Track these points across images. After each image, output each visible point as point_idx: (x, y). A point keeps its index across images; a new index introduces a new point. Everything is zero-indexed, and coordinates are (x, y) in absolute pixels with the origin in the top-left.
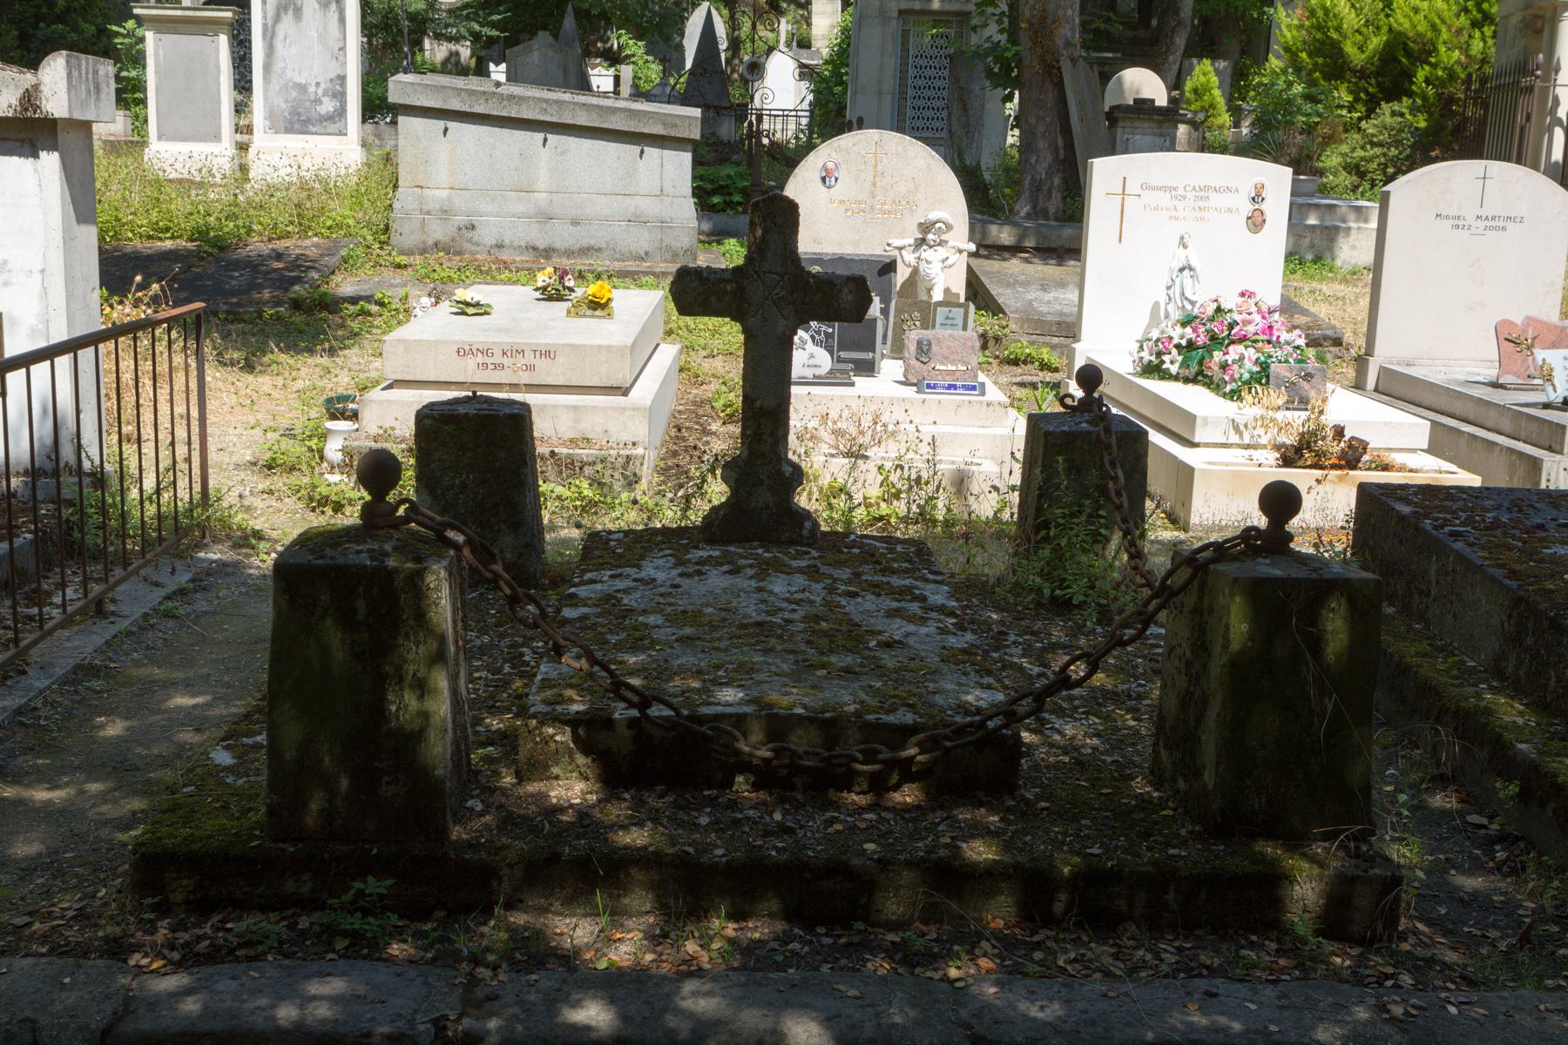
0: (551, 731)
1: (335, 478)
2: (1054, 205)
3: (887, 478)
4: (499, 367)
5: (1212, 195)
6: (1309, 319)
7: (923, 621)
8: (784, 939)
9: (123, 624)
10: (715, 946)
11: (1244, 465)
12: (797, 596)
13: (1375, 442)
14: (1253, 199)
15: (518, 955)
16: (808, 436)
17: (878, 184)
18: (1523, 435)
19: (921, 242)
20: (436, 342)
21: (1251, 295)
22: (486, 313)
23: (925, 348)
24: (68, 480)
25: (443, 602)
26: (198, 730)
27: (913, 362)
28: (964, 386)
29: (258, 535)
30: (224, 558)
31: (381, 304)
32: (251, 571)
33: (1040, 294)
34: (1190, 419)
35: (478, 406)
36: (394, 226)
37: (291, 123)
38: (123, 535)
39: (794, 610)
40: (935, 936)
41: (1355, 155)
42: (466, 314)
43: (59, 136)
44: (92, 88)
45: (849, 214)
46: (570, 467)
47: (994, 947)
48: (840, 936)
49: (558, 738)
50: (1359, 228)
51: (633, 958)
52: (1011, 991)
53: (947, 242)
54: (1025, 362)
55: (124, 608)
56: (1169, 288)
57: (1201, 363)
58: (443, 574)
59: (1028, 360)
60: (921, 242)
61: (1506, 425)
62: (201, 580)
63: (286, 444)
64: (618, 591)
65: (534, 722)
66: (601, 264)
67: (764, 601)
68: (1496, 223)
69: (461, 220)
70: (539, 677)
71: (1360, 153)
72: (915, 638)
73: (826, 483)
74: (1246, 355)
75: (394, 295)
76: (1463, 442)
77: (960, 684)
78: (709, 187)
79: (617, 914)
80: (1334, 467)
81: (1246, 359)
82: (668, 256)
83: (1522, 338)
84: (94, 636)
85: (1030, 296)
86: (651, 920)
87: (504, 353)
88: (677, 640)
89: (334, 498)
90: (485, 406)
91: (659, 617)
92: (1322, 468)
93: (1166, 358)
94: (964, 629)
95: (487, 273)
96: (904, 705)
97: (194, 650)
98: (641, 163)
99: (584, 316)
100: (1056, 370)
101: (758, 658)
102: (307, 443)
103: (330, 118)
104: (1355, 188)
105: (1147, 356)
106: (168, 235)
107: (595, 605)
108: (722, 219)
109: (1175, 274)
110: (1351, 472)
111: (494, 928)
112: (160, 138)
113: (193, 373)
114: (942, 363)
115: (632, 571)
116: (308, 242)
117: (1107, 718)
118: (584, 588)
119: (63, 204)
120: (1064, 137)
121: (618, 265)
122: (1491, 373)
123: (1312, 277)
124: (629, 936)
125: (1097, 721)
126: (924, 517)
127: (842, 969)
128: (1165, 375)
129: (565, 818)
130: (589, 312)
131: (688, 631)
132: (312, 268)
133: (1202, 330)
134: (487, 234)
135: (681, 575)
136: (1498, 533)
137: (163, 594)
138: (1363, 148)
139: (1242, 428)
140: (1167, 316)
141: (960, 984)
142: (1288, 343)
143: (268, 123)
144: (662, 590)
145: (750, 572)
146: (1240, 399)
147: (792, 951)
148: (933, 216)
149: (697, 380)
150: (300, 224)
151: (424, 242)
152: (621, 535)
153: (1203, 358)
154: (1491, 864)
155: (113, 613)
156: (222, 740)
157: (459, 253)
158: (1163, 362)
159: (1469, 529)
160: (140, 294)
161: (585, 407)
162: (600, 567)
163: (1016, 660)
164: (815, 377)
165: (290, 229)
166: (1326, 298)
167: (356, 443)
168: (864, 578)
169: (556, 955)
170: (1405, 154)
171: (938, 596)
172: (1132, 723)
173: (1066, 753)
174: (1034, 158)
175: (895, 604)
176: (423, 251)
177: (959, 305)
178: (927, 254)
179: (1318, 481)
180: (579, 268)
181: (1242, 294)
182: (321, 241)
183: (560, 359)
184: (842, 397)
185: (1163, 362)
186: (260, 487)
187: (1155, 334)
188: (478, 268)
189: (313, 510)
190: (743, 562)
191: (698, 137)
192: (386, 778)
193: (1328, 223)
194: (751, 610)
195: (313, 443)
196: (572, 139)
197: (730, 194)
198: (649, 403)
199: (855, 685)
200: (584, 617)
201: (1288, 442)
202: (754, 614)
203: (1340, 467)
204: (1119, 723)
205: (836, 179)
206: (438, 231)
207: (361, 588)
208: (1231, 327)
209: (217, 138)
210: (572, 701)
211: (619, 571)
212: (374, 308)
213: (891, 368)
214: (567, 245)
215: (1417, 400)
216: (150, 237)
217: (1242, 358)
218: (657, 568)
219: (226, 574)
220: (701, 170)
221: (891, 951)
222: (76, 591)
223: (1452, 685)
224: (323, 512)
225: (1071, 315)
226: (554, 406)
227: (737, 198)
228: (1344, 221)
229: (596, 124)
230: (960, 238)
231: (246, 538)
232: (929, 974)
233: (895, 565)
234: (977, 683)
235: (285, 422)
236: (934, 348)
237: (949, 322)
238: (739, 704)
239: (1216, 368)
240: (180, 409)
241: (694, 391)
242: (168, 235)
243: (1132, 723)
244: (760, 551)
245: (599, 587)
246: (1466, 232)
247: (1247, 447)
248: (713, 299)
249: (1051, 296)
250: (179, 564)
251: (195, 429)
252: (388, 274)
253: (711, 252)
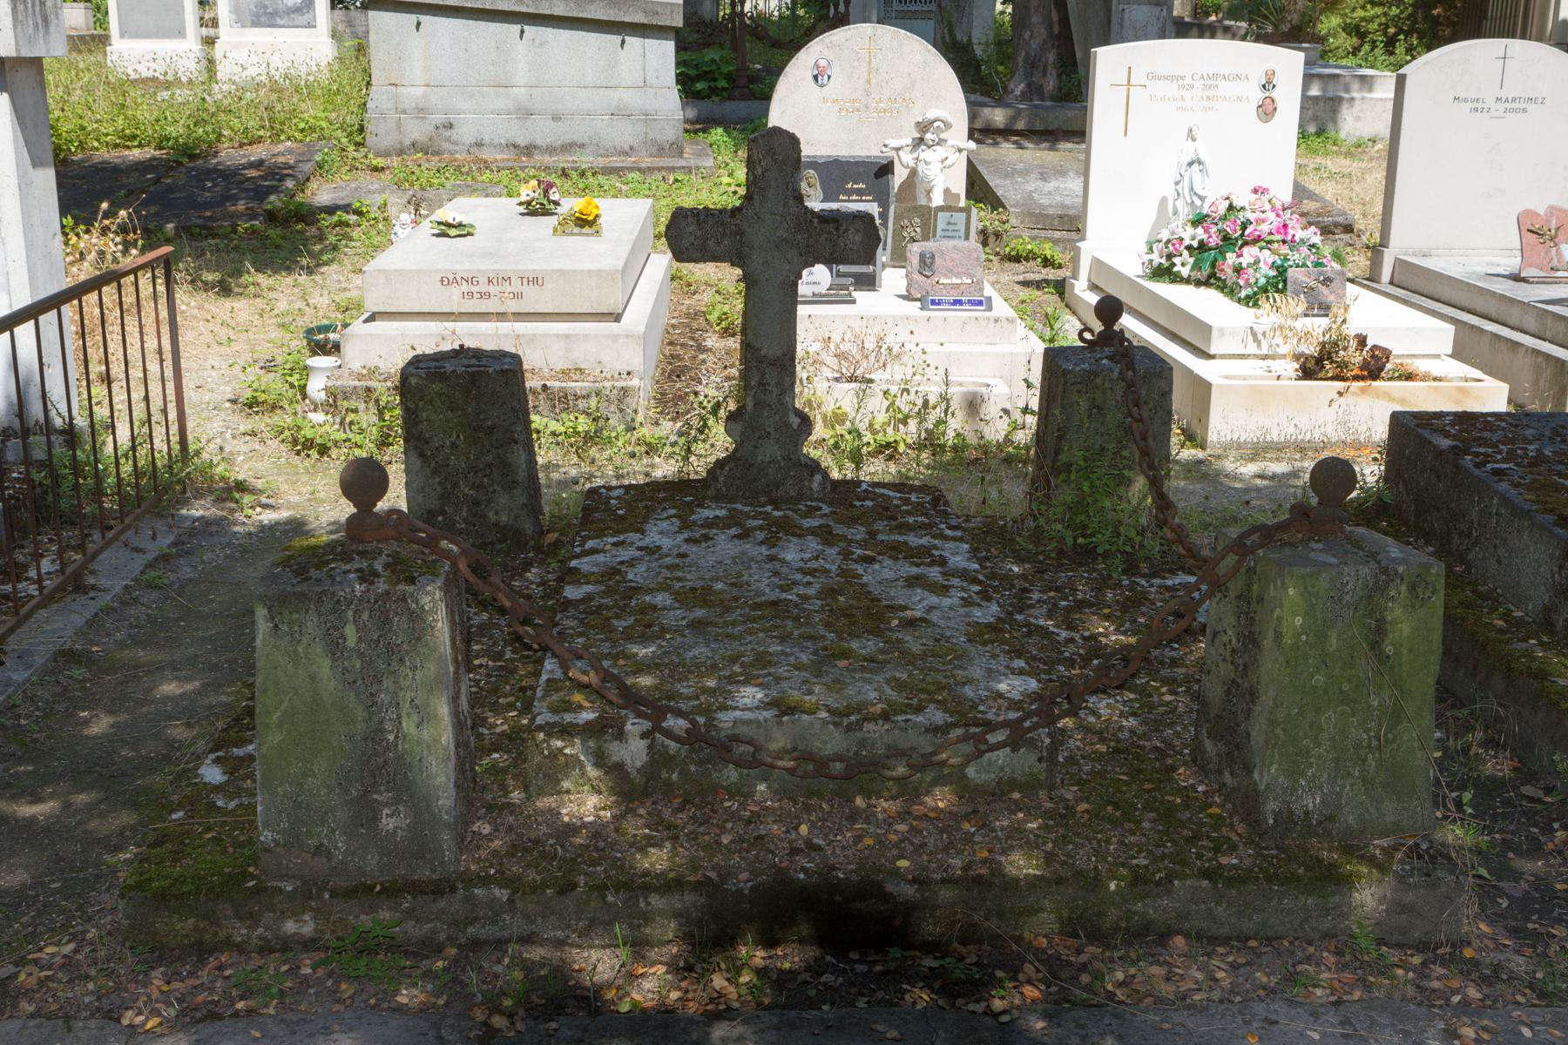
0: (559, 744)
1: (319, 417)
2: (1050, 84)
3: (893, 403)
5: (1221, 83)
6: (1318, 205)
7: (944, 590)
8: (816, 968)
9: (104, 600)
10: (745, 979)
11: (1263, 378)
12: (814, 564)
13: (1398, 347)
14: (1264, 86)
15: (535, 998)
16: (810, 361)
17: (874, 81)
18: (1548, 335)
19: (920, 141)
20: (419, 271)
21: (1264, 191)
22: (469, 234)
23: (928, 261)
24: (37, 440)
25: (440, 624)
26: (188, 725)
27: (916, 276)
28: (970, 302)
29: (241, 487)
30: (207, 514)
31: (359, 213)
32: (237, 529)
33: (1040, 183)
34: (1206, 329)
35: (466, 362)
36: (369, 127)
37: (258, 16)
38: (98, 492)
39: (809, 584)
40: (975, 959)
41: (1355, 15)
42: (448, 236)
43: (8, 76)
44: (40, 21)
45: (843, 113)
46: (562, 401)
47: (1038, 971)
48: (874, 963)
49: (567, 751)
50: (1363, 99)
51: (656, 997)
52: (1059, 1025)
53: (946, 141)
54: (1027, 259)
55: (104, 582)
56: (1177, 183)
57: (1213, 265)
58: (438, 595)
59: (1030, 257)
60: (920, 141)
61: (1531, 323)
62: (183, 543)
63: (267, 378)
64: (622, 563)
65: (541, 735)
66: (585, 160)
67: (776, 573)
68: (1515, 105)
69: (438, 118)
70: (544, 677)
71: (1360, 13)
72: (938, 613)
73: (830, 410)
74: (1262, 258)
75: (371, 202)
76: (1486, 340)
77: (990, 671)
78: (693, 72)
79: (639, 947)
80: (1356, 378)
81: (1258, 261)
82: (654, 150)
83: (1545, 229)
84: (74, 616)
85: (1030, 187)
86: (675, 950)
88: (687, 626)
89: (319, 441)
90: (473, 361)
91: (666, 595)
92: (1344, 379)
93: (1177, 260)
94: (989, 599)
95: (467, 174)
96: (933, 701)
97: (179, 626)
98: (622, 53)
99: (572, 234)
100: (1060, 266)
101: (775, 648)
102: (288, 378)
104: (1355, 51)
105: (1157, 259)
106: (136, 143)
107: (598, 582)
108: (707, 105)
109: (1184, 168)
110: (1375, 384)
111: (508, 967)
112: (122, 36)
113: (163, 302)
114: (946, 276)
115: (633, 537)
116: (281, 147)
117: (1143, 691)
118: (586, 559)
119: (16, 148)
120: (1058, 11)
121: (602, 162)
122: (1512, 263)
123: (1315, 152)
124: (652, 971)
125: (1132, 696)
126: (930, 442)
127: (879, 1002)
128: (1176, 279)
129: (578, 841)
130: (577, 230)
131: (700, 613)
132: (290, 175)
133: (1214, 229)
134: (466, 132)
135: (687, 541)
136: (1543, 468)
137: (145, 562)
138: (1363, 7)
139: (1260, 336)
140: (1175, 213)
141: (1005, 1018)
142: (1303, 241)
143: (234, 17)
144: (668, 561)
145: (761, 536)
146: (1256, 305)
147: (825, 984)
148: (931, 115)
149: (689, 289)
150: (272, 128)
151: (401, 143)
152: (622, 491)
153: (1216, 260)
154: (1551, 846)
155: (93, 587)
156: (212, 751)
157: (438, 153)
158: (1174, 265)
159: (1512, 465)
160: (107, 222)
161: (576, 335)
162: (600, 534)
163: (1041, 622)
164: (814, 295)
165: (261, 133)
166: (1331, 176)
167: (339, 383)
168: (880, 537)
169: (575, 997)
170: (1406, 13)
171: (959, 555)
172: (1168, 698)
173: (1102, 740)
174: (1028, 33)
175: (914, 570)
176: (401, 152)
177: (961, 210)
178: (925, 154)
179: (1340, 394)
180: (562, 165)
181: (1255, 191)
182: (295, 145)
183: (549, 286)
184: (843, 317)
185: (1174, 265)
186: (242, 428)
187: (1165, 235)
188: (458, 169)
189: (298, 453)
190: (752, 523)
191: (680, 25)
192: (386, 811)
193: (1330, 94)
194: (762, 584)
195: (294, 379)
196: (550, 30)
197: (715, 80)
198: (642, 329)
199: (879, 678)
200: (588, 598)
201: (1307, 352)
202: (767, 591)
203: (1363, 378)
204: (1156, 698)
205: (829, 77)
206: (416, 131)
207: (350, 613)
208: (1244, 226)
209: (181, 34)
210: (581, 707)
211: (622, 538)
212: (353, 218)
213: (893, 279)
214: (548, 141)
215: (1436, 296)
216: (116, 146)
217: (1257, 262)
218: (661, 533)
219: (211, 534)
220: (685, 56)
221: (929, 979)
222: (53, 561)
223: (1500, 641)
224: (308, 456)
225: (1073, 207)
226: (544, 336)
227: (723, 83)
228: (1347, 90)
229: (574, 14)
230: (958, 135)
231: (229, 490)
232: (971, 1007)
233: (911, 520)
234: (1007, 667)
235: (265, 351)
236: (938, 261)
237: (951, 227)
238: (757, 708)
239: (1230, 271)
240: (151, 344)
241: (687, 302)
242: (136, 143)
243: (1168, 698)
244: (769, 509)
245: (601, 558)
246: (1485, 115)
247: (1265, 357)
249: (1051, 186)
250: (160, 525)
251: (168, 364)
252: (365, 179)
253: (697, 143)
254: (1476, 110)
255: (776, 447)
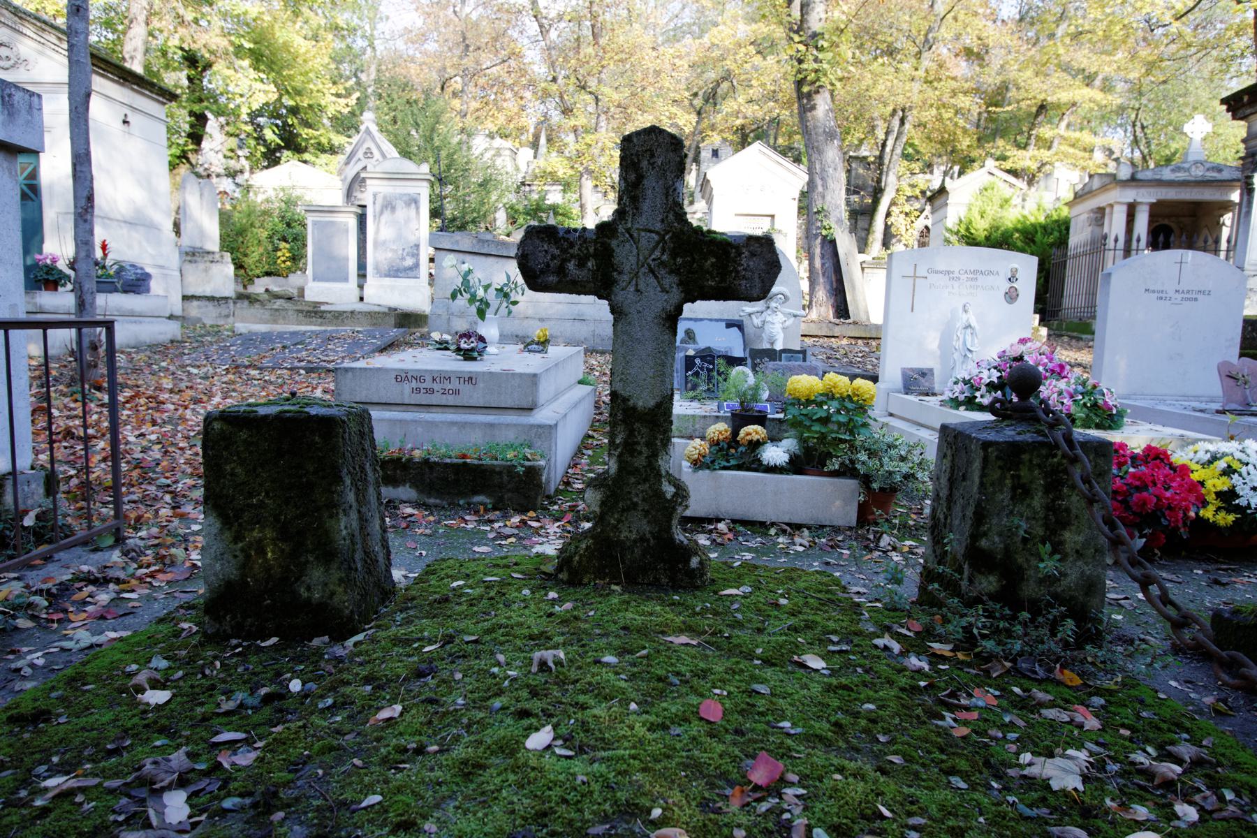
4: (430, 391)
87: (434, 380)
103: (410, 269)
209: (346, 279)
246: (1168, 302)
248: (571, 265)
254: (1161, 298)
255: (645, 522)
